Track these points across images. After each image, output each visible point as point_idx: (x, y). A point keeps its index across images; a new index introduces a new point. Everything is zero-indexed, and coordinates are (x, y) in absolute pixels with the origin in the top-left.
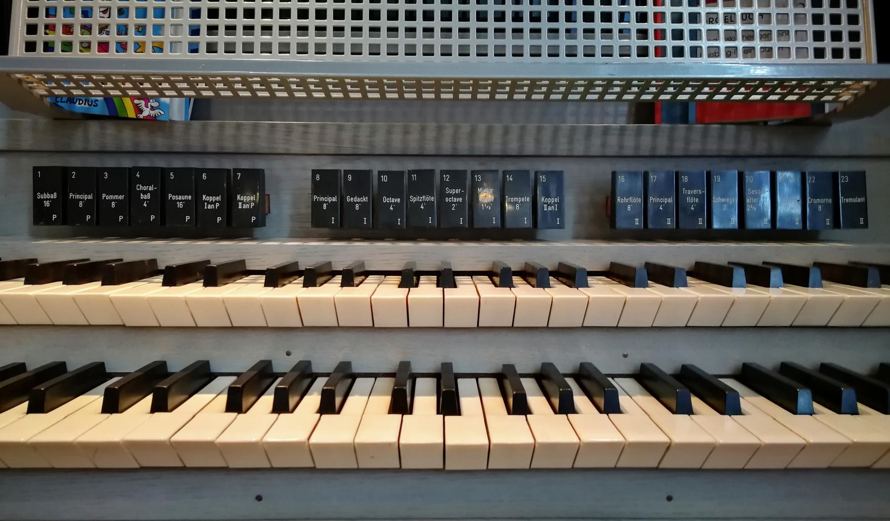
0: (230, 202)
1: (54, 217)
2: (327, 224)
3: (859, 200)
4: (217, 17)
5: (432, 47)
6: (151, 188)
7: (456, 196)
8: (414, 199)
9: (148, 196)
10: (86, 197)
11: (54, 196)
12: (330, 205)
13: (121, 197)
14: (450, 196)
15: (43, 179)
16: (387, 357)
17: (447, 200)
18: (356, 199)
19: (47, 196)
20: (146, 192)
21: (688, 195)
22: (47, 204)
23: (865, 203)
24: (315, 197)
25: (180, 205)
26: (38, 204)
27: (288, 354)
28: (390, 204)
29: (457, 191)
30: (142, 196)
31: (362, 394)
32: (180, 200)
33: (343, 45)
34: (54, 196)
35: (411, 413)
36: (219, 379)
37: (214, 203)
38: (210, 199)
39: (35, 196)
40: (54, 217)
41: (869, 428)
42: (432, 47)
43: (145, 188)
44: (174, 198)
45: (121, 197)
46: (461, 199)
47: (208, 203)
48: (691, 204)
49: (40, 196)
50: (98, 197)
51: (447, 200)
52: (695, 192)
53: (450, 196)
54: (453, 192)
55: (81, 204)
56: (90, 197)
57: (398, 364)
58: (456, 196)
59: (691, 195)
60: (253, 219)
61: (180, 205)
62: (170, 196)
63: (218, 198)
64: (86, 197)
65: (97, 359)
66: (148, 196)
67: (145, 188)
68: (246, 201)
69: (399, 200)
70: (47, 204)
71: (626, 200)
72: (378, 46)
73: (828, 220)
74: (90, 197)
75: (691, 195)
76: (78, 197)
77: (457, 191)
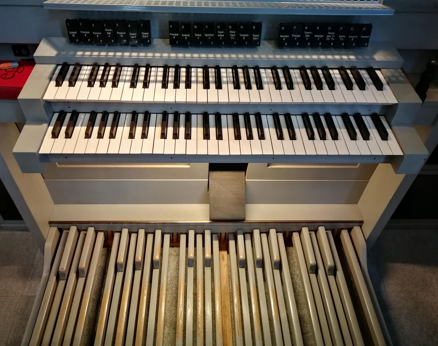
1: (77, 40)
3: (367, 37)
6: (110, 30)
7: (222, 34)
8: (206, 35)
9: (110, 33)
10: (87, 33)
14: (219, 34)
17: (218, 35)
19: (73, 33)
22: (74, 36)
23: (368, 39)
24: (171, 34)
28: (198, 36)
29: (222, 32)
30: (306, 36)
31: (121, 126)
32: (121, 34)
34: (76, 33)
35: (115, 138)
37: (147, 35)
38: (133, 34)
43: (108, 30)
44: (95, 33)
45: (100, 33)
46: (223, 35)
47: (132, 36)
51: (218, 35)
52: (309, 33)
53: (219, 34)
54: (221, 32)
55: (244, 38)
58: (222, 34)
60: (149, 41)
64: (87, 33)
66: (110, 33)
67: (108, 30)
70: (74, 36)
74: (88, 33)
77: (222, 32)
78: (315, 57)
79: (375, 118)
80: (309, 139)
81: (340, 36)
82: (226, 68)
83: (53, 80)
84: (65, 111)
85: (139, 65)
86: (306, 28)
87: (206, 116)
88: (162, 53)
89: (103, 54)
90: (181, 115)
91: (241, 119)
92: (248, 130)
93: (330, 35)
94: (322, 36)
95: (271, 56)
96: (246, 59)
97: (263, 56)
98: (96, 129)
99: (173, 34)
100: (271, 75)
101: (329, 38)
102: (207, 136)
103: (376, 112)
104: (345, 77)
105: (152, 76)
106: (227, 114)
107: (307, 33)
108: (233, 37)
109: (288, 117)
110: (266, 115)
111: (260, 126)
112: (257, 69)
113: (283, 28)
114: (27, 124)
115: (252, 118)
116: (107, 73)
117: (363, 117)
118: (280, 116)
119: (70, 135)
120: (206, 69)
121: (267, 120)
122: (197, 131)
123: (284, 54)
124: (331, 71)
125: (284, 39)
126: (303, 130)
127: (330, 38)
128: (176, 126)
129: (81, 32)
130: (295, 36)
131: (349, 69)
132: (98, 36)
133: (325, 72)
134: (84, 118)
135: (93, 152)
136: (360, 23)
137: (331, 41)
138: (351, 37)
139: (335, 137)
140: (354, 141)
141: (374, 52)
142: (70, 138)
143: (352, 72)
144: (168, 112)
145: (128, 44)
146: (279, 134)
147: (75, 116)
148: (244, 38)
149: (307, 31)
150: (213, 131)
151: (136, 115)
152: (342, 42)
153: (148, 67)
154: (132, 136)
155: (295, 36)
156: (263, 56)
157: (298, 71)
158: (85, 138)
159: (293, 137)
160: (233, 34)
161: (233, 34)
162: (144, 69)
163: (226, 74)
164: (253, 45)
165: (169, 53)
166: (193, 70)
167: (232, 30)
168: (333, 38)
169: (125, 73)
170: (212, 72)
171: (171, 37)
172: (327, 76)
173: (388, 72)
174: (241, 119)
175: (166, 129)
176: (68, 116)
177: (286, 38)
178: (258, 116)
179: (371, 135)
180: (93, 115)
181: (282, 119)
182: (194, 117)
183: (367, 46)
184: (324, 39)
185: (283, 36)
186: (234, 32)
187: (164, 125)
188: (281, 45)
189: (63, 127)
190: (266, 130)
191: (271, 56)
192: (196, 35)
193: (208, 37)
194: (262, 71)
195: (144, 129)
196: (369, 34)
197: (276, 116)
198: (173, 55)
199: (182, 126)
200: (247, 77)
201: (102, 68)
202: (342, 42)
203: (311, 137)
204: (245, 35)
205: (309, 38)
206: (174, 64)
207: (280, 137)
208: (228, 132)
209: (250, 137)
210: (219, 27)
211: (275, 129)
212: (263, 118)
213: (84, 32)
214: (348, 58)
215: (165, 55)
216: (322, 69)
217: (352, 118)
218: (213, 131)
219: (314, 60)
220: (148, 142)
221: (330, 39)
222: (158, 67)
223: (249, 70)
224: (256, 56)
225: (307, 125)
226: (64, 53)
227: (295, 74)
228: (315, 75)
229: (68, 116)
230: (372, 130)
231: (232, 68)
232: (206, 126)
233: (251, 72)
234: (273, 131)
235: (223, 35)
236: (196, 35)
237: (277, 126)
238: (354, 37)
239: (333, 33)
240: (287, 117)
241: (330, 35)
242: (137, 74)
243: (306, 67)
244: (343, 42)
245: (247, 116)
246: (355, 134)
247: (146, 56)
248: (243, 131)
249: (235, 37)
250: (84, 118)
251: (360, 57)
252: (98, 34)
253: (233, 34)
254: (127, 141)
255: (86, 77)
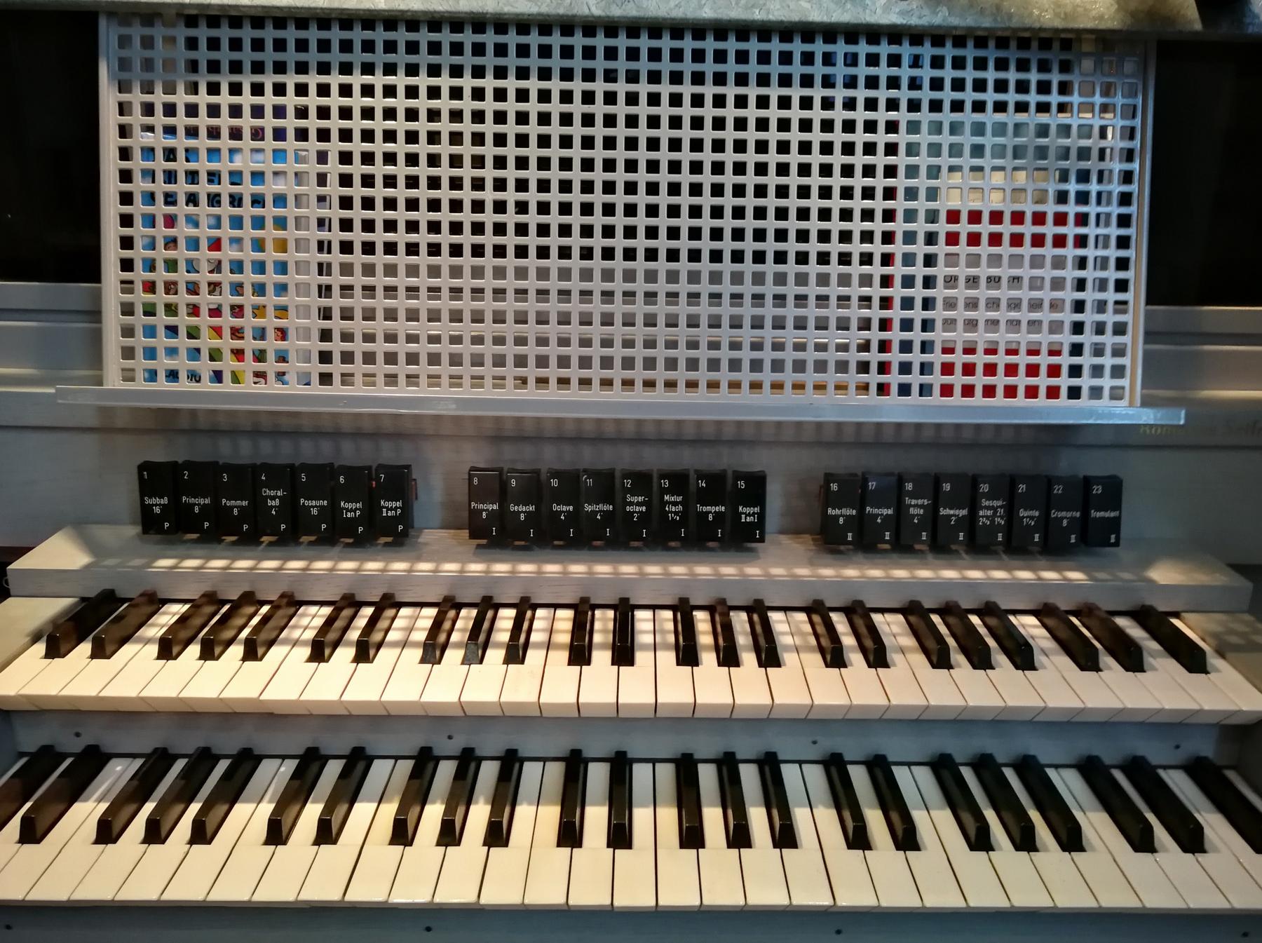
0: (372, 509)
1: (167, 525)
2: (160, 531)
3: (1113, 514)
4: (806, 285)
5: (719, 317)
6: (279, 493)
7: (639, 504)
10: (202, 501)
11: (165, 501)
12: (490, 513)
13: (245, 503)
14: (631, 504)
15: (153, 478)
16: (673, 745)
17: (628, 508)
18: (522, 508)
19: (156, 501)
20: (274, 498)
21: (911, 506)
22: (157, 510)
24: (473, 504)
25: (315, 512)
26: (146, 511)
27: (450, 737)
28: (562, 512)
29: (641, 499)
30: (270, 503)
32: (314, 505)
33: (698, 316)
34: (165, 501)
36: (114, 762)
38: (350, 506)
39: (142, 501)
40: (167, 525)
41: (1217, 875)
42: (654, 316)
43: (272, 493)
45: (245, 503)
46: (644, 509)
47: (348, 510)
48: (914, 516)
49: (148, 501)
50: (216, 501)
51: (628, 508)
52: (920, 502)
53: (631, 504)
54: (635, 499)
55: (197, 510)
56: (207, 501)
57: (418, 749)
58: (639, 504)
59: (915, 506)
60: (400, 527)
61: (315, 512)
62: (302, 501)
63: (399, 504)
64: (202, 501)
65: (202, 744)
67: (272, 493)
68: (390, 508)
69: (571, 508)
70: (157, 510)
71: (837, 512)
72: (762, 317)
73: (850, 534)
74: (207, 501)
75: (915, 506)
76: (192, 500)
77: (641, 499)
78: (950, 574)
79: (1204, 773)
80: (851, 846)
81: (1022, 513)
82: (654, 608)
83: (239, 643)
84: (108, 748)
85: (497, 600)
86: (909, 486)
87: (575, 765)
88: (442, 562)
89: (373, 566)
90: (591, 766)
91: (707, 776)
92: (775, 813)
93: (988, 508)
94: (964, 512)
95: (803, 571)
96: (720, 581)
97: (777, 571)
98: (433, 814)
99: (481, 506)
100: (808, 628)
101: (987, 517)
102: (692, 837)
103: (1203, 754)
104: (1064, 634)
105: (538, 630)
106: (654, 761)
107: (914, 502)
108: (676, 513)
109: (879, 768)
110: (800, 763)
111: (776, 797)
112: (758, 610)
113: (834, 487)
114: (362, 801)
115: (749, 776)
116: (447, 625)
117: (1051, 773)
118: (850, 768)
119: (209, 831)
120: (684, 610)
121: (804, 781)
122: (535, 819)
123: (845, 567)
124: (877, 618)
125: (841, 520)
126: (944, 817)
127: (991, 518)
128: (732, 799)
129: (184, 499)
130: (876, 511)
131: (1076, 613)
132: (236, 511)
133: (992, 621)
134: (274, 775)
135: (554, 897)
136: (1081, 476)
137: (993, 529)
138: (1061, 514)
139: (1071, 840)
140: (981, 856)
141: (1148, 562)
142: (334, 842)
143: (1047, 621)
144: (479, 753)
145: (337, 534)
146: (850, 825)
147: (358, 763)
148: (1065, 523)
149: (913, 495)
150: (596, 818)
151: (473, 766)
152: (919, 529)
153: (525, 607)
154: (402, 834)
155: (876, 511)
156: (777, 571)
157: (900, 617)
158: (394, 841)
159: (906, 839)
160: (675, 504)
161: (675, 504)
162: (512, 613)
163: (789, 629)
164: (742, 538)
165: (464, 562)
166: (640, 614)
167: (671, 491)
168: (1002, 517)
169: (305, 621)
170: (604, 620)
171: (474, 514)
172: (1001, 632)
173: (1212, 622)
174: (707, 776)
175: (507, 810)
176: (333, 769)
177: (847, 518)
178: (770, 766)
179: (1088, 832)
180: (425, 762)
181: (859, 777)
182: (641, 773)
183: (1117, 544)
184: (971, 522)
185: (837, 512)
186: (680, 499)
187: (416, 793)
188: (831, 540)
189: (309, 806)
190: (801, 815)
191: (803, 571)
192: (556, 508)
193: (594, 513)
194: (775, 616)
195: (450, 810)
196: (1117, 506)
197: (835, 766)
198: (476, 568)
199: (482, 800)
200: (725, 633)
201: (368, 611)
202: (1030, 531)
203: (980, 841)
204: (713, 509)
205: (921, 517)
206: (474, 595)
207: (858, 839)
208: (654, 820)
209: (739, 838)
210: (628, 483)
211: (833, 812)
212: (789, 773)
213: (192, 500)
214: (1067, 578)
215: (451, 567)
216: (942, 612)
217: (968, 774)
218: (596, 818)
219: (950, 584)
220: (337, 856)
221: (993, 521)
222: (556, 606)
223: (732, 614)
224: (753, 571)
225: (957, 798)
226: (110, 562)
227: (892, 627)
228: (959, 630)
229: (333, 769)
230: (1090, 814)
231: (808, 610)
232: (572, 798)
233: (740, 621)
234: (827, 817)
235: (644, 509)
236: (556, 508)
237: (843, 798)
238: (1069, 514)
239: (1000, 503)
240: (767, 769)
241: (988, 508)
242: (486, 625)
243: (927, 605)
244: (1034, 529)
245: (728, 766)
246: (1149, 829)
247: (487, 572)
248: (713, 819)
249: (684, 515)
250: (274, 775)
251: (1101, 575)
252: (236, 505)
253: (674, 505)
254: (383, 853)
255: (310, 635)
